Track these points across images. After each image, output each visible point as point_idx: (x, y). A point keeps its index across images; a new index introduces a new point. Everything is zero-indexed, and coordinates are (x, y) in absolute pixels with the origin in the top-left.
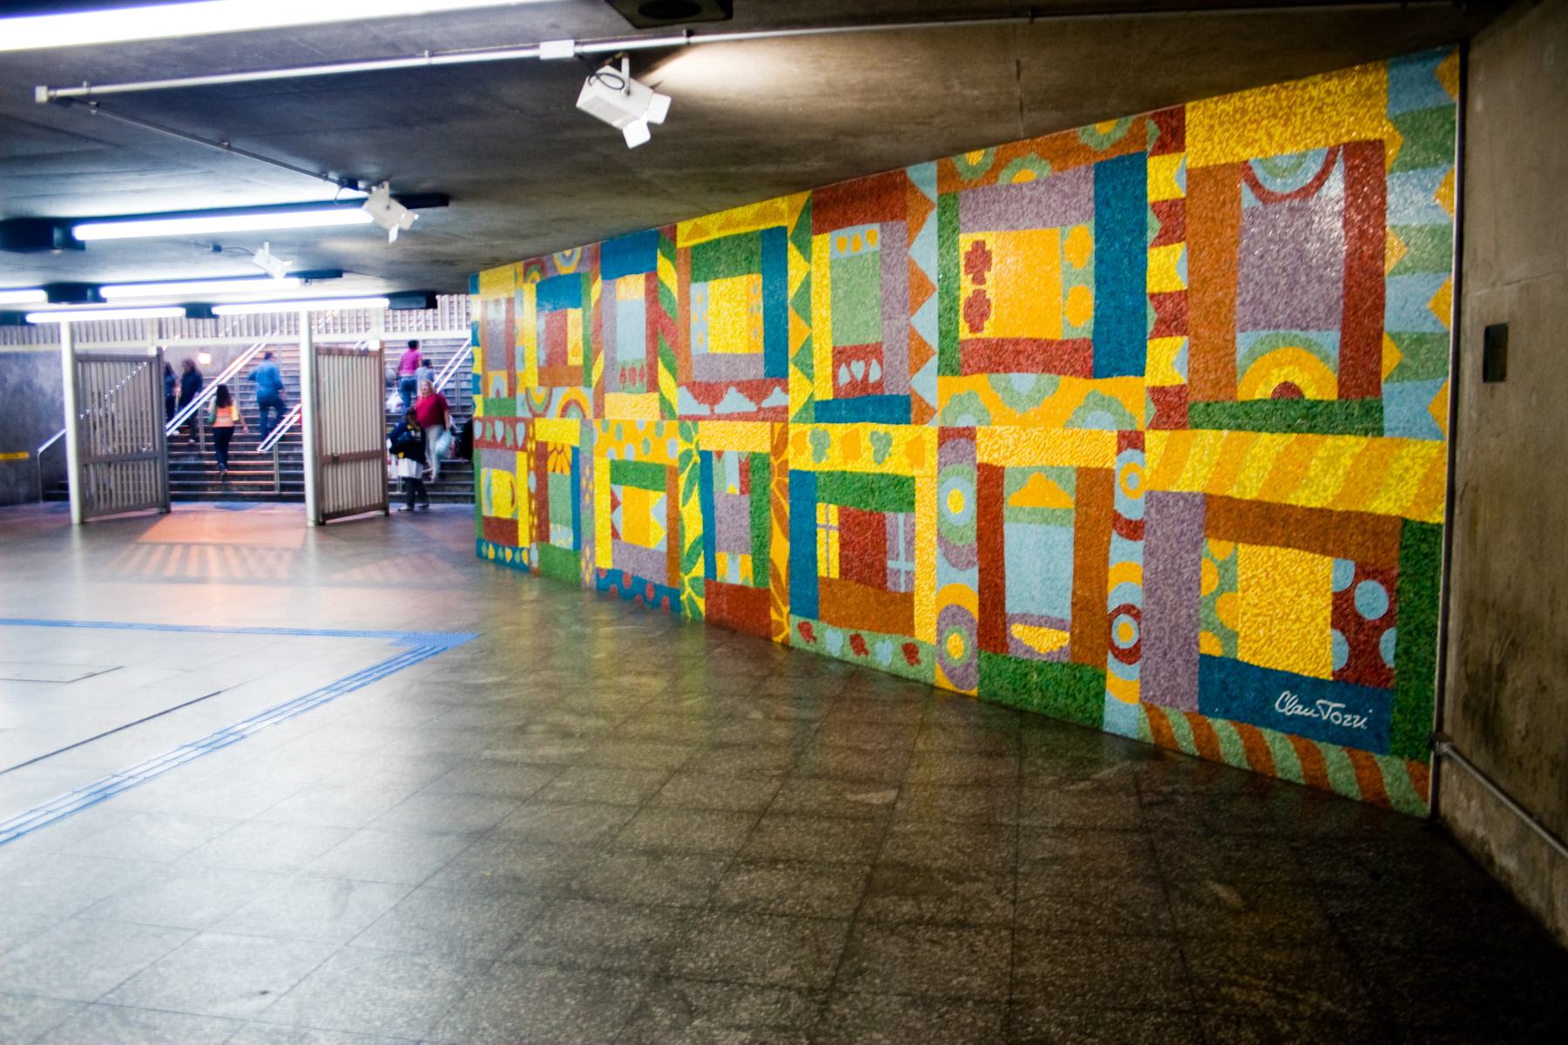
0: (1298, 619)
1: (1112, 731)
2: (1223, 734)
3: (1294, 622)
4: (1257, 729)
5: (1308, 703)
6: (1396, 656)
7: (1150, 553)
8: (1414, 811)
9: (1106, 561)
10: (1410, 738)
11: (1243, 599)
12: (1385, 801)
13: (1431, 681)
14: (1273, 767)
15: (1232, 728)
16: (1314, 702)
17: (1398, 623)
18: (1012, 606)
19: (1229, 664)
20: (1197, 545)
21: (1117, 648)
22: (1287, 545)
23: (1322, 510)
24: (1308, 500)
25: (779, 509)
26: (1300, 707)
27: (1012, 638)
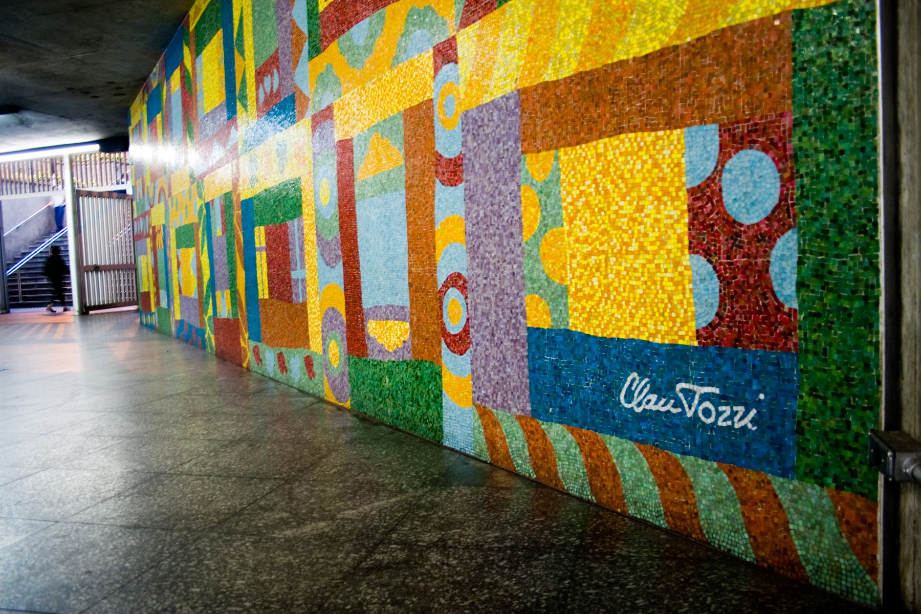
0: (642, 247)
1: (451, 446)
2: (559, 447)
3: (637, 255)
4: (600, 435)
5: (663, 390)
6: (801, 285)
7: (470, 198)
8: (849, 591)
9: (432, 223)
10: (836, 445)
11: (569, 234)
12: (795, 565)
13: (871, 326)
14: (623, 497)
15: (570, 437)
16: (673, 388)
17: (801, 219)
18: (367, 302)
19: (559, 339)
20: (514, 168)
21: (449, 335)
22: (619, 130)
23: (662, 52)
24: (642, 44)
25: (238, 241)
26: (654, 397)
27: (369, 338)
